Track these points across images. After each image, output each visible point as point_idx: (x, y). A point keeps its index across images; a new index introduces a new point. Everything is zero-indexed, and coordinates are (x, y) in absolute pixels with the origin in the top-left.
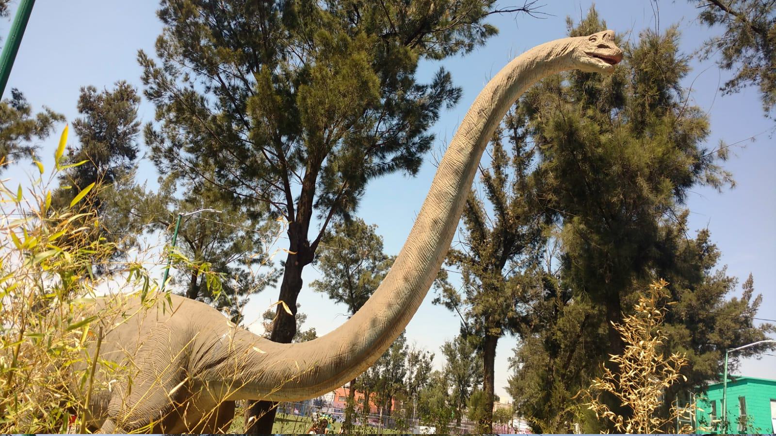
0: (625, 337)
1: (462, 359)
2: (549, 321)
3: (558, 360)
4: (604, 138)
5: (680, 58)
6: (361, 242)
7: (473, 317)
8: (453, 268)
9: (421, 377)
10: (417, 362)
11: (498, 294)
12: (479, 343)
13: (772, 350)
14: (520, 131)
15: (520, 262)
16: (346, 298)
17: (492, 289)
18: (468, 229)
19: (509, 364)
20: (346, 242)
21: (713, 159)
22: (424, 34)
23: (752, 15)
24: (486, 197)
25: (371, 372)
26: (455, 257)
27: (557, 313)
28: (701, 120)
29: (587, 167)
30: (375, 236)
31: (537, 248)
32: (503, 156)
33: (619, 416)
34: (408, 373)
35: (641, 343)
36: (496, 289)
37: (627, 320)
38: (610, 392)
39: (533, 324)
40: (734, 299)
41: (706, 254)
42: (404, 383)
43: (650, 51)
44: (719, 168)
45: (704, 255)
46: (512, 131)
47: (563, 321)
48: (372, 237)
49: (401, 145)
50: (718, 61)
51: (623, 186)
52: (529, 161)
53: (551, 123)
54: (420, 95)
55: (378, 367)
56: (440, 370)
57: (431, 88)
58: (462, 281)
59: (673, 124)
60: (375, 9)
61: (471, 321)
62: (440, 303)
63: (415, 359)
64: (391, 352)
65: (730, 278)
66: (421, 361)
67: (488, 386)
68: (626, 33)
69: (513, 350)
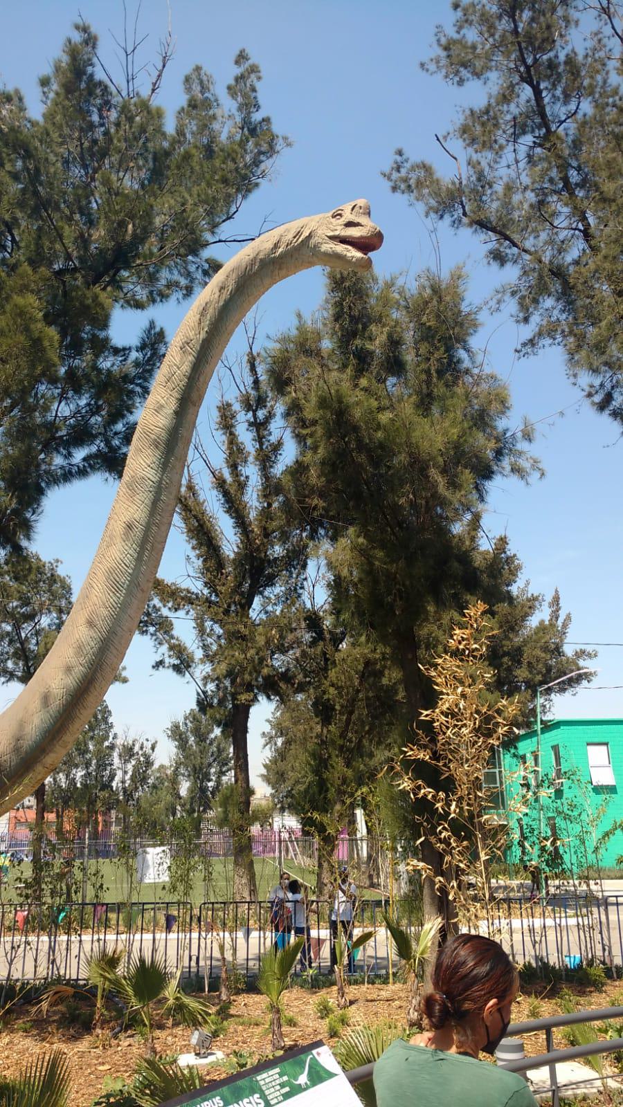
0: (437, 685)
1: (197, 744)
2: (317, 675)
3: (332, 728)
4: (384, 417)
5: (467, 310)
6: (36, 588)
7: (213, 681)
8: (181, 613)
9: (140, 777)
10: (131, 756)
11: (247, 645)
12: (224, 717)
13: (588, 681)
14: (261, 414)
15: (273, 597)
16: (20, 674)
17: (237, 638)
18: (198, 557)
19: (263, 741)
20: (13, 589)
21: (517, 442)
22: (118, 270)
23: (548, 253)
24: (221, 509)
25: (63, 780)
26: (183, 598)
27: (327, 662)
28: (499, 390)
29: (362, 458)
30: (59, 576)
31: (294, 576)
32: (240, 451)
33: (440, 793)
34: (119, 774)
35: (459, 690)
36: (244, 638)
37: (440, 661)
38: (426, 762)
39: (297, 681)
40: (542, 622)
41: (506, 567)
42: (114, 789)
43: (432, 299)
44: (525, 453)
45: (504, 569)
46: (250, 414)
47: (336, 673)
48: (53, 579)
49: (95, 437)
50: (513, 313)
51: (413, 483)
52: (276, 456)
53: (314, 400)
54: (121, 361)
55: (74, 771)
56: (167, 763)
57: (137, 351)
58: (195, 632)
59: (467, 397)
60: (40, 229)
61: (211, 687)
62: (164, 667)
63: (128, 752)
64: (91, 747)
65: (535, 595)
66: (137, 753)
67: (240, 777)
68: (401, 274)
69: (268, 721)
